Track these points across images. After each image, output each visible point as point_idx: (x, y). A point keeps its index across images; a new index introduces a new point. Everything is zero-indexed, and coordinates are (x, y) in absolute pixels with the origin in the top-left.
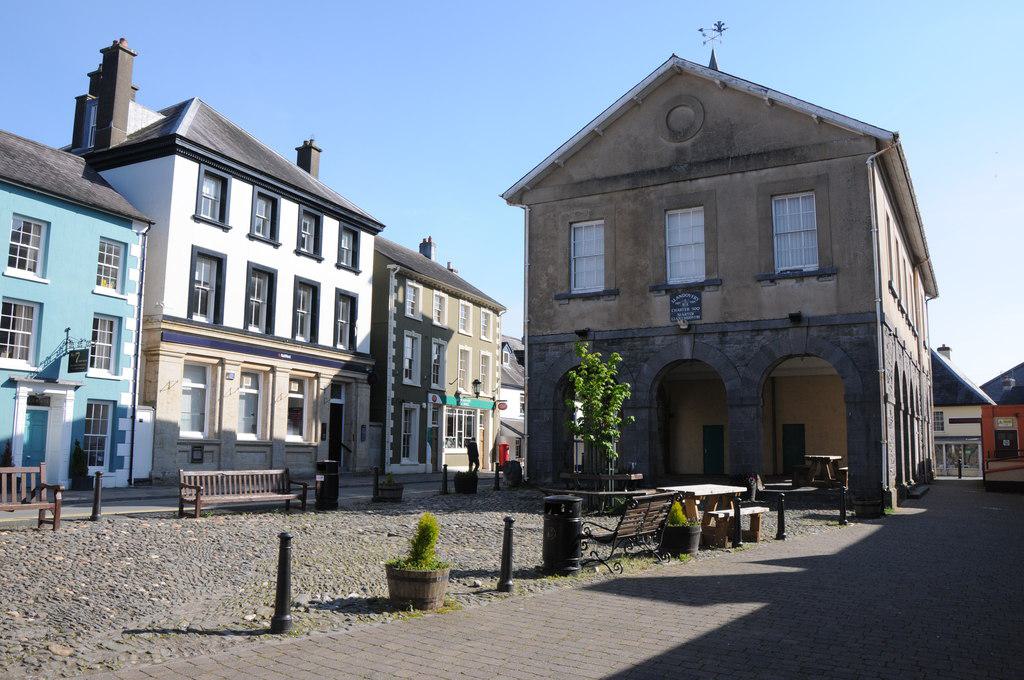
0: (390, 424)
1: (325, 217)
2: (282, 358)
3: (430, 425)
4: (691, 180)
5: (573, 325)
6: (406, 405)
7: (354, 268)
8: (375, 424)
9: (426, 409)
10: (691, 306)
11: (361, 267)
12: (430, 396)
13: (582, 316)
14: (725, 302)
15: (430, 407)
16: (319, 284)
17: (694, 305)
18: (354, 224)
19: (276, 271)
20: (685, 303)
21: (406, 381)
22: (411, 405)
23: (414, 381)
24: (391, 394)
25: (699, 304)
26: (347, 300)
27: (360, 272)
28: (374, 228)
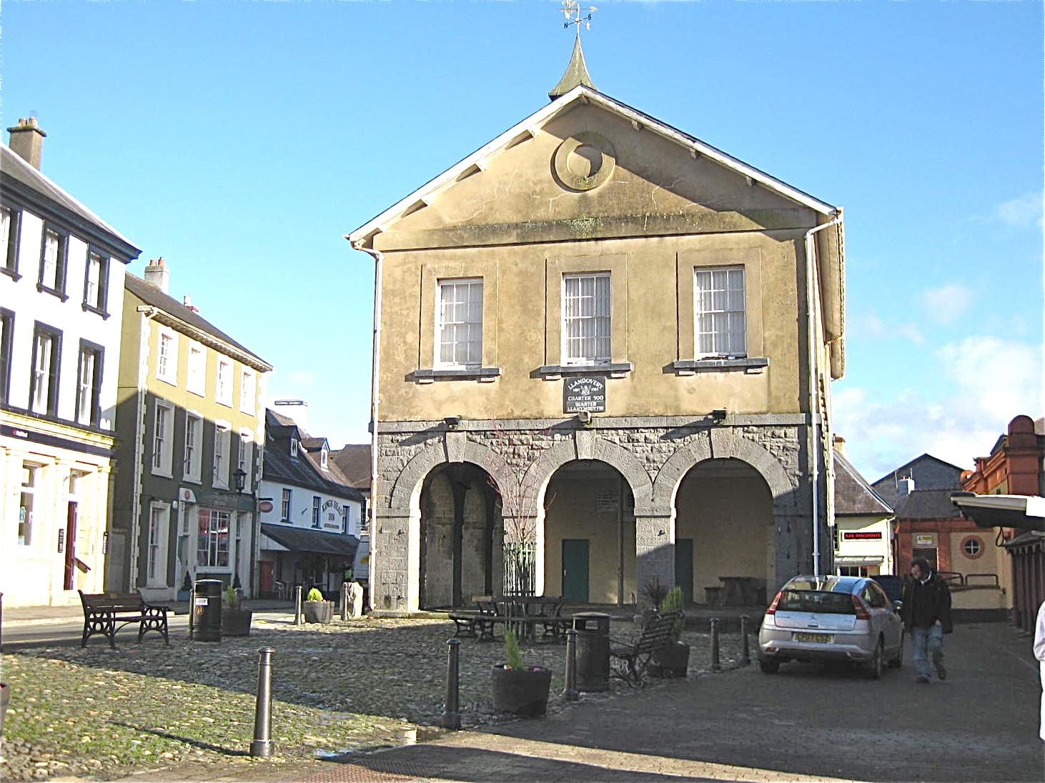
0: (136, 530)
1: (71, 237)
2: (563, 570)
3: (180, 533)
4: (597, 239)
5: (439, 410)
6: (154, 504)
7: (101, 309)
8: (117, 530)
9: (177, 511)
10: (592, 394)
11: (69, 291)
12: (182, 491)
13: (453, 399)
14: (634, 392)
15: (182, 507)
16: (61, 332)
17: (598, 394)
18: (106, 246)
19: (61, 332)
20: (585, 391)
21: (155, 471)
22: (160, 504)
23: (164, 469)
24: (138, 489)
25: (603, 392)
26: (92, 351)
27: (68, 297)
28: (129, 253)
